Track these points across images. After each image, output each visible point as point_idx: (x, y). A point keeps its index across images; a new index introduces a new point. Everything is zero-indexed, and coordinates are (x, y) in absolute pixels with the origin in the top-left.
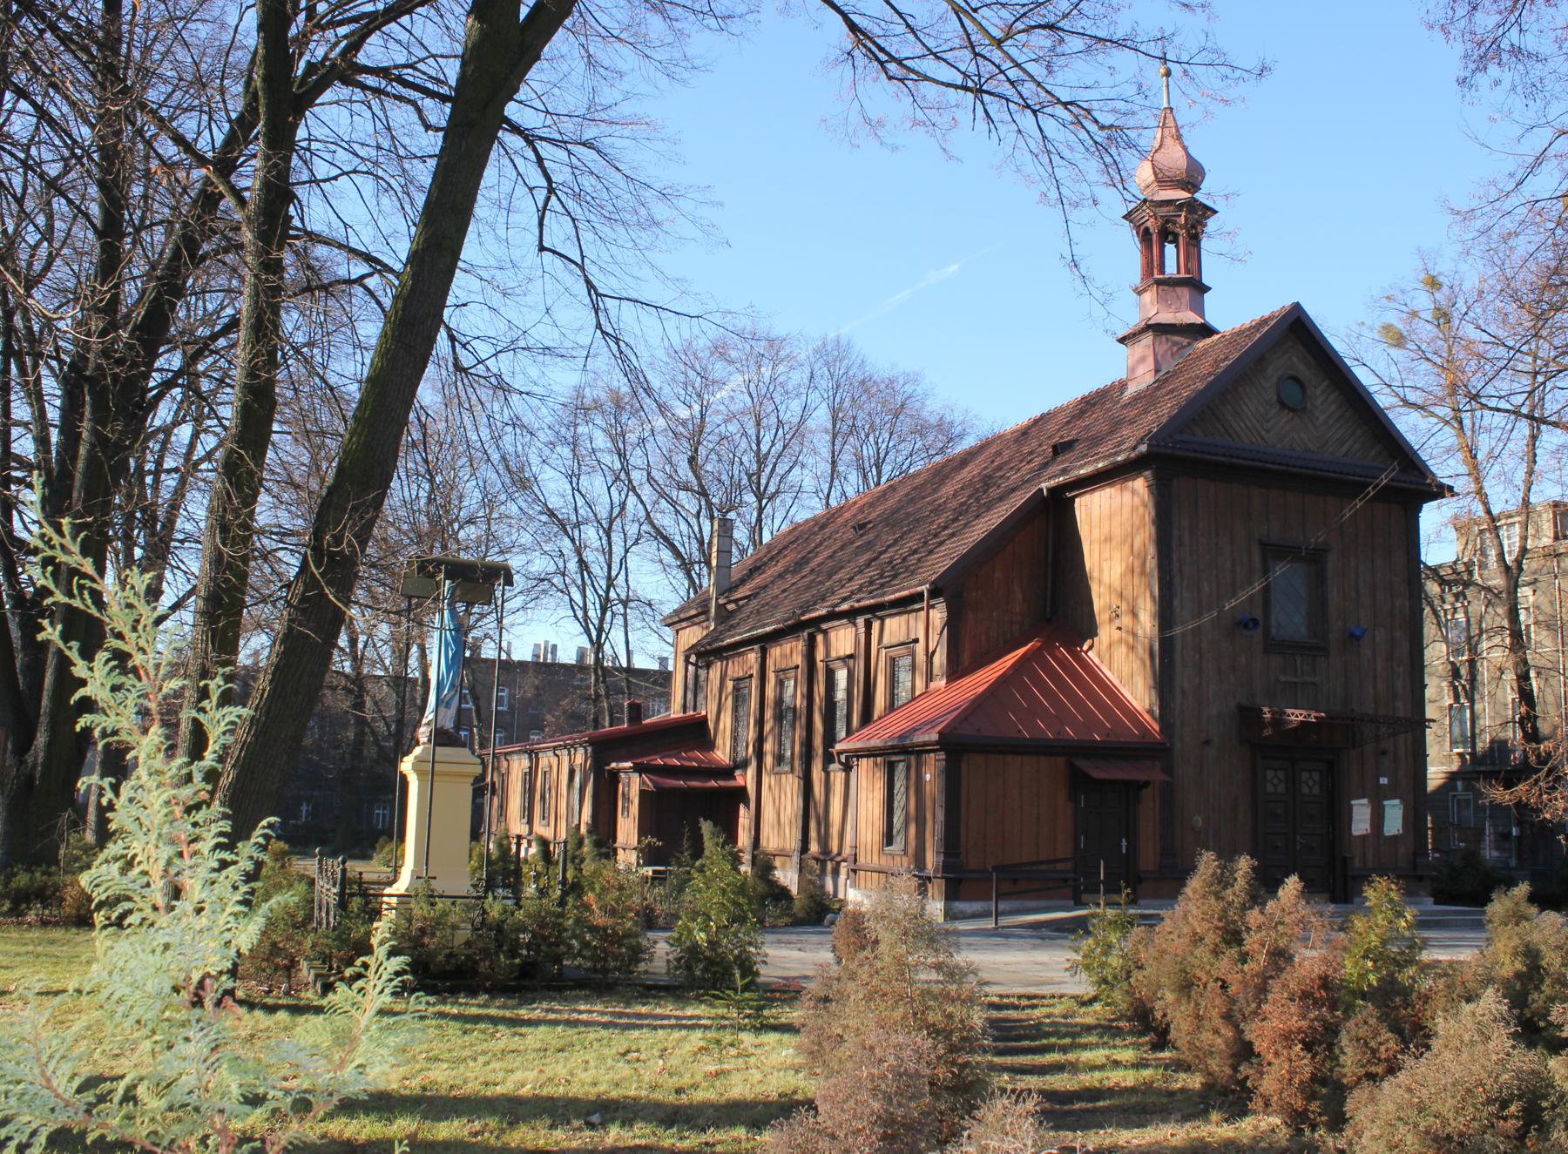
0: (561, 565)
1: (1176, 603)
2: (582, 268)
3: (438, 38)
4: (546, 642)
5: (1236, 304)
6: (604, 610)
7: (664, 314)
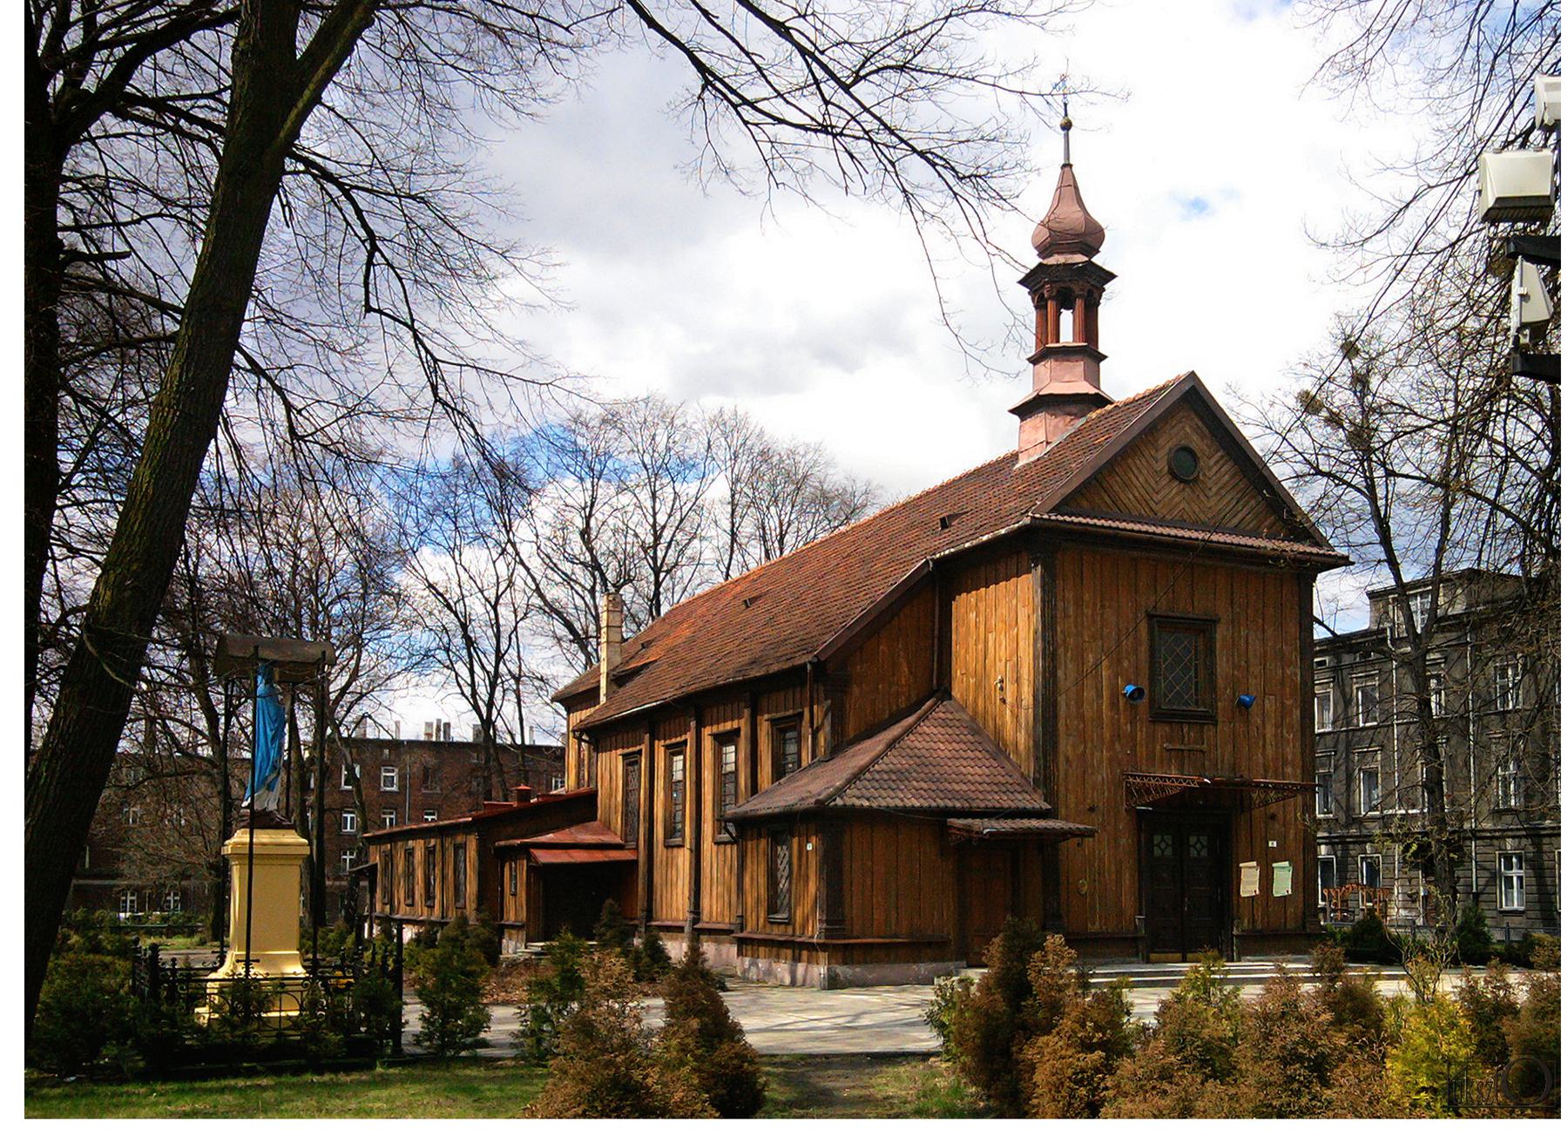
0: (446, 640)
1: (1060, 673)
2: (411, 328)
3: (202, 66)
4: (439, 721)
5: (1132, 368)
6: (493, 686)
7: (509, 381)
